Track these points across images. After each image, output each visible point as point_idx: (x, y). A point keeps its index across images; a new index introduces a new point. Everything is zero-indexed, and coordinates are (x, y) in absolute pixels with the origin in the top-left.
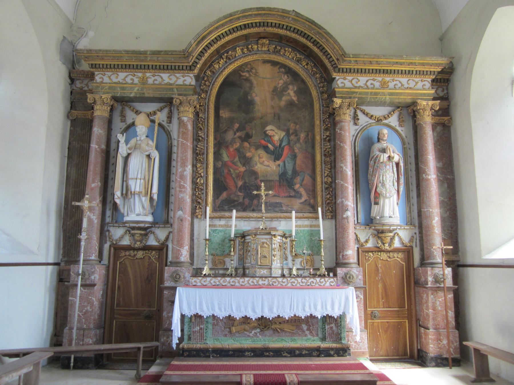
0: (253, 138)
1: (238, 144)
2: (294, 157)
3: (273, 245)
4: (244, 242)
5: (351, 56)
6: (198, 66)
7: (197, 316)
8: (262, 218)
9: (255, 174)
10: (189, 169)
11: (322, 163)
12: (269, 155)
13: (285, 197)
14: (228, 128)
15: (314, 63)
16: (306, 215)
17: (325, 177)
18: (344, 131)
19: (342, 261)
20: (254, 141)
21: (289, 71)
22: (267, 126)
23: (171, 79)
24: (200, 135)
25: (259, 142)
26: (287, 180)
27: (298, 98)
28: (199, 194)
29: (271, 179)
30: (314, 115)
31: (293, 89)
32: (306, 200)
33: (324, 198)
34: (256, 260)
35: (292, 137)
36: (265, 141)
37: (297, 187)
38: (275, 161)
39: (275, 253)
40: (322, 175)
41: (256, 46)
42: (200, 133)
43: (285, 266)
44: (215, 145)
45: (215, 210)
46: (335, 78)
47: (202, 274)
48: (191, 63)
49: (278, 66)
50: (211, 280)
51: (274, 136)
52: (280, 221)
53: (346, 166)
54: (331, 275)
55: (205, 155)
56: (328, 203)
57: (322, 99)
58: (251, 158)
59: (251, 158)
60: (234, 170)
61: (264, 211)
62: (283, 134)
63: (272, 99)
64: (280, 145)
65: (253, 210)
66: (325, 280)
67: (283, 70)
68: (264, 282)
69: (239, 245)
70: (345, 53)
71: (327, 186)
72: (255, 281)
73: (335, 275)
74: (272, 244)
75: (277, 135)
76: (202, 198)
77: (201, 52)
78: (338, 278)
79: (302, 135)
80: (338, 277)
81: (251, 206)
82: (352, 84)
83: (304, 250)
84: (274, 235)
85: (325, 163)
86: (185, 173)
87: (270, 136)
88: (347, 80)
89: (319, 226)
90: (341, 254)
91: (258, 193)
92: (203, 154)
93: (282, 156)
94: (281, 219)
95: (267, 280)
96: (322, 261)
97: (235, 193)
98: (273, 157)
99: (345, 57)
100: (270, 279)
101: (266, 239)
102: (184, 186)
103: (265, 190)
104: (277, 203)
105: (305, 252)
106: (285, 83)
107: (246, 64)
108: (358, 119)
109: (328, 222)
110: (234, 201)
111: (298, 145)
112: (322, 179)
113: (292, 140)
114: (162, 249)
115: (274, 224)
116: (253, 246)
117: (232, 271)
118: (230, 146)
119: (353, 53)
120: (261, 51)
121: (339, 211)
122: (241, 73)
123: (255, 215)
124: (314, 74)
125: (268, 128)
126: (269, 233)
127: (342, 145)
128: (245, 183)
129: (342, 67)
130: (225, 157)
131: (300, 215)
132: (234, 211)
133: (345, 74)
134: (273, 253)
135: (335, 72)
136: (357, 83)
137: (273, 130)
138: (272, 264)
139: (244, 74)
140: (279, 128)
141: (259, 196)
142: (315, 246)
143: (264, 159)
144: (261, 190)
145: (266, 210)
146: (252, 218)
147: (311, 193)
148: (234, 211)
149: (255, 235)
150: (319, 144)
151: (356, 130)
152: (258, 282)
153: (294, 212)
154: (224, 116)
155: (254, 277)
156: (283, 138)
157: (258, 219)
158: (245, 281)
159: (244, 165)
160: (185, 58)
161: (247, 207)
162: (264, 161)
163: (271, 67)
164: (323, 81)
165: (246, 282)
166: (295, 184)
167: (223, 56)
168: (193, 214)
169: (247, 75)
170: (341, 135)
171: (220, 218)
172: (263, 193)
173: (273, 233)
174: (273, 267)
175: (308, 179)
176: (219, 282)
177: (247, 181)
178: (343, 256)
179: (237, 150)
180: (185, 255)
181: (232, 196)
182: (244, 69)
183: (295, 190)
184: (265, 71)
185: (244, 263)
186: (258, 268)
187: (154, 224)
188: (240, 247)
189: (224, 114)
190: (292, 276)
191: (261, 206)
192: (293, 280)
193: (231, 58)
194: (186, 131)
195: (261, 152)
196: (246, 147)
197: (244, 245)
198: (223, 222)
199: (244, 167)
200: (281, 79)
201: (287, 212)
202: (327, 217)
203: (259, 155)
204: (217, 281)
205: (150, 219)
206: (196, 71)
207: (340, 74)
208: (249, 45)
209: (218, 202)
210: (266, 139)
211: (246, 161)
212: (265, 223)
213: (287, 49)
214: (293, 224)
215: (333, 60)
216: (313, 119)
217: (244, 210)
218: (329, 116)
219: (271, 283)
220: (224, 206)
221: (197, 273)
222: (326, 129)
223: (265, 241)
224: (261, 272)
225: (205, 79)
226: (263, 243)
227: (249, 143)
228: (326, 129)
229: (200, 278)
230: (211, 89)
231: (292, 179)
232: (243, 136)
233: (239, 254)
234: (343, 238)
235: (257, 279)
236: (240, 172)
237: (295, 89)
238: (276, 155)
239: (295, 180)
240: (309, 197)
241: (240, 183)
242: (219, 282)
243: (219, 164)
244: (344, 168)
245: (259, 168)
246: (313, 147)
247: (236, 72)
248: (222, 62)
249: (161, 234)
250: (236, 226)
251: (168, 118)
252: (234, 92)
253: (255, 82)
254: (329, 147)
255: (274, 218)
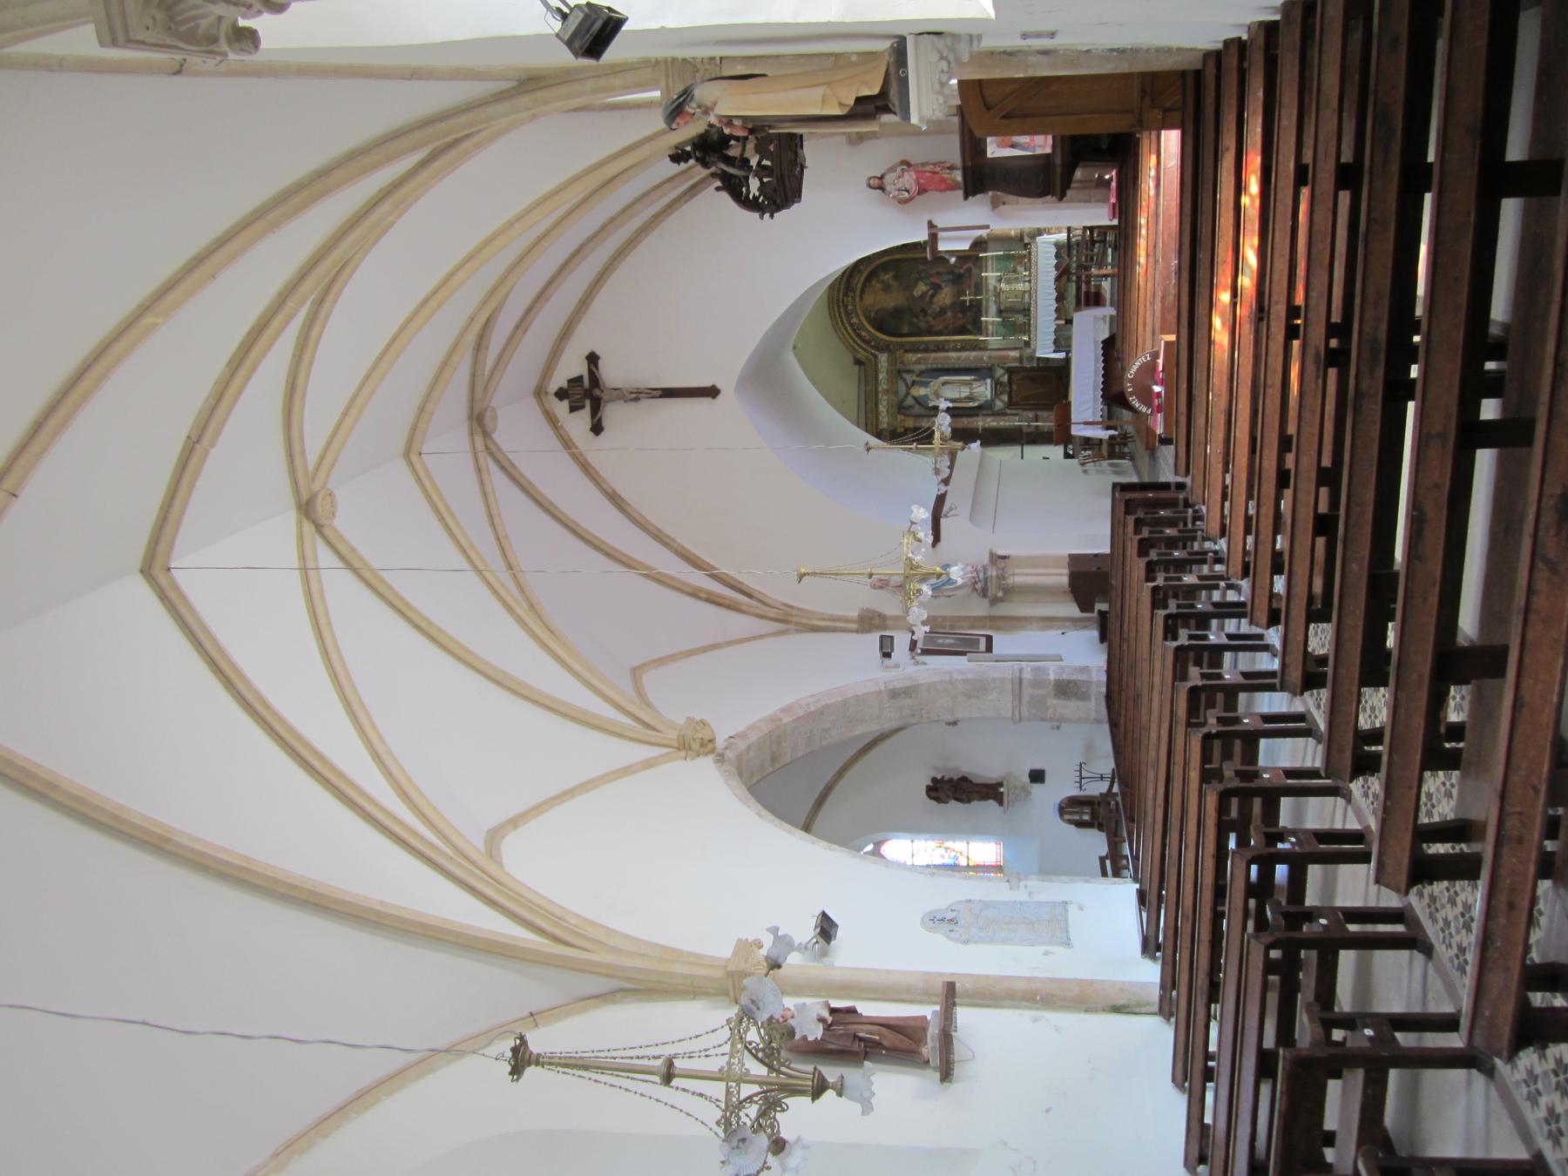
7: (1055, 342)
9: (953, 304)
75: (921, 288)
97: (968, 318)
114: (1011, 371)
126: (998, 293)
168: (985, 349)
180: (1015, 354)
184: (869, 299)
187: (992, 377)
189: (906, 329)
205: (989, 381)
211: (943, 311)
214: (991, 275)
216: (908, 260)
220: (978, 328)
221: (1027, 344)
238: (937, 288)
245: (948, 301)
249: (999, 372)
252: (886, 322)
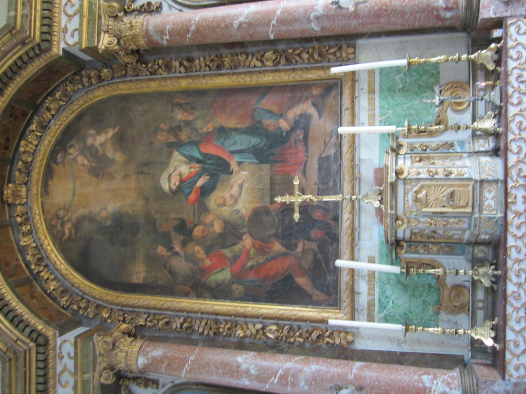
0: (185, 217)
1: (197, 248)
2: (222, 131)
3: (421, 176)
4: (410, 242)
5: (13, 14)
6: (40, 327)
8: (352, 202)
9: (257, 215)
10: (246, 360)
11: (234, 74)
12: (219, 184)
13: (307, 151)
14: (165, 267)
15: (46, 98)
16: (346, 103)
17: (264, 65)
18: (165, 25)
19: (461, 12)
20: (191, 215)
21: (62, 144)
22: (162, 189)
23: (67, 383)
24: (179, 325)
25: (193, 204)
26: (270, 147)
27: (110, 127)
28: (300, 336)
29: (267, 181)
30: (141, 94)
31: (93, 136)
32: (314, 105)
33: (309, 66)
34: (459, 216)
35: (184, 137)
36: (190, 192)
37: (284, 125)
38: (231, 173)
39: (440, 171)
40: (260, 72)
41: (19, 208)
42: (174, 326)
43: (468, 148)
44: (199, 296)
45: (334, 303)
46: (63, 50)
47: (493, 348)
48: (32, 344)
49: (54, 165)
50: (513, 330)
51: (180, 175)
52: (360, 160)
53: (237, 16)
54: (497, 33)
55: (218, 317)
56: (320, 55)
57: (112, 79)
58: (226, 222)
59: (226, 222)
60: (249, 258)
61: (337, 198)
62: (177, 156)
63: (111, 177)
64: (199, 161)
65: (336, 219)
66: (513, 48)
67: (59, 156)
68: (520, 200)
69: (416, 252)
70: (7, 26)
71: (283, 61)
72: (517, 221)
73: (499, 23)
74: (419, 180)
75: (179, 168)
76: (310, 329)
77: (11, 321)
78: (509, 14)
79: (180, 116)
80: (505, 14)
81: (327, 224)
82: (75, 14)
83: (433, 104)
84: (397, 174)
85: (236, 68)
86: (253, 372)
87: (182, 181)
88: (68, 26)
89: (371, 72)
90: (443, 14)
91: (297, 209)
92: (217, 322)
93: (220, 158)
94: (357, 159)
95: (513, 191)
96: (459, 59)
98: (222, 177)
99: (14, 28)
100: (510, 184)
101: (405, 194)
102: (281, 377)
103: (292, 194)
104: (320, 169)
105: (437, 101)
106: (82, 152)
107: (50, 228)
108: (149, 4)
109: (361, 54)
110: (316, 261)
111: (199, 124)
112: (267, 71)
113: (189, 137)
115: (367, 173)
116: (424, 224)
117: (486, 274)
118: (201, 265)
119: (6, 10)
120: (27, 198)
121: (339, 27)
122: (65, 237)
123: (346, 216)
124: (65, 96)
125: (166, 187)
126: (389, 186)
127: (193, 28)
128: (276, 236)
129: (38, 33)
130: (224, 275)
131: (346, 116)
132: (339, 263)
133: (55, 29)
134: (441, 175)
135: (49, 49)
136: (73, 6)
137: (170, 175)
138: (470, 179)
139: (67, 232)
140: (165, 164)
141: (305, 208)
142: (421, 80)
143: (227, 195)
144: (292, 204)
145: (335, 193)
146: (353, 222)
147: (298, 95)
148: (339, 263)
149: (397, 219)
150: (197, 81)
151: (170, 6)
152: (518, 214)
153: (341, 130)
154: (142, 275)
155: (505, 224)
156: (186, 156)
157: (355, 210)
158: (517, 247)
159: (240, 238)
160: (17, 359)
161: (328, 234)
162: (231, 196)
163: (55, 179)
164: (78, 77)
165: (519, 243)
166: (280, 128)
167: (36, 271)
169: (69, 225)
170: (173, 30)
171: (353, 293)
172: (297, 199)
173: (392, 177)
174: (476, 176)
175: (268, 102)
176: (517, 309)
177: (273, 231)
178: (447, 9)
179: (208, 250)
181: (306, 264)
182: (58, 231)
183: (292, 130)
184: (62, 191)
185: (460, 243)
186: (480, 211)
188: (422, 251)
189: (139, 273)
190: (500, 130)
191: (326, 202)
192: (513, 126)
193: (39, 256)
194: (166, 362)
195: (212, 201)
196: (203, 231)
197: (412, 242)
198: (362, 287)
199: (244, 237)
200: (75, 160)
201: (340, 146)
202: (351, 56)
203: (219, 206)
204: (515, 315)
206: (50, 332)
207: (55, 38)
208: (16, 221)
209: (317, 294)
210: (187, 191)
211: (231, 232)
212: (366, 196)
213: (22, 149)
214: (368, 132)
215: (27, 53)
217: (336, 239)
218: (142, 63)
219: (521, 182)
220: (327, 287)
222: (168, 67)
223: (410, 197)
224: (489, 206)
225: (75, 307)
226: (416, 200)
227: (196, 225)
228: (168, 67)
229: (508, 356)
230: (94, 297)
231: (267, 137)
232: (182, 237)
233: (438, 253)
234: (403, 13)
235: (510, 216)
236: (254, 246)
237: (93, 132)
238: (218, 169)
239: (271, 129)
240: (307, 98)
241: (277, 247)
242: (517, 309)
243: (238, 289)
244: (241, 19)
245: (245, 206)
246: (202, 93)
247: (63, 247)
248: (44, 275)
250: (371, 260)
251: (146, 386)
253: (81, 212)
254: (202, 59)
255: (353, 174)
